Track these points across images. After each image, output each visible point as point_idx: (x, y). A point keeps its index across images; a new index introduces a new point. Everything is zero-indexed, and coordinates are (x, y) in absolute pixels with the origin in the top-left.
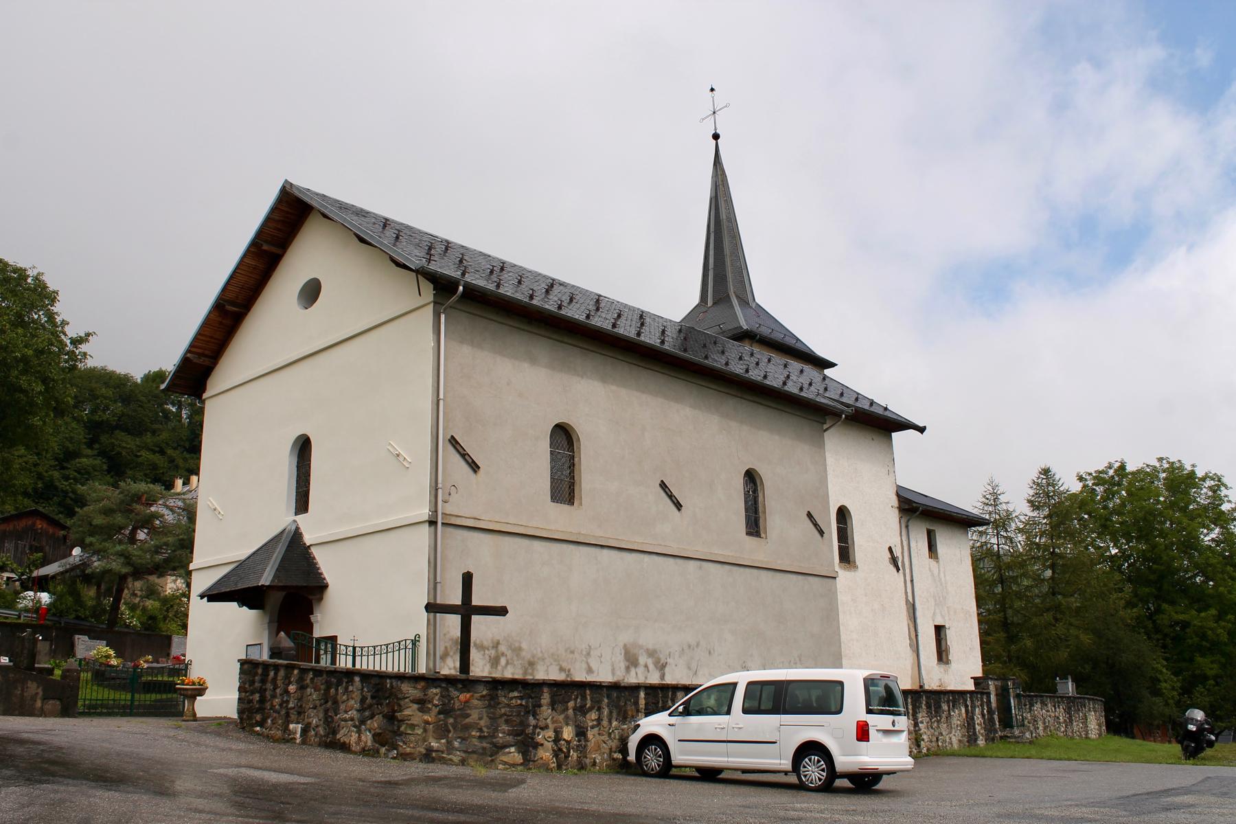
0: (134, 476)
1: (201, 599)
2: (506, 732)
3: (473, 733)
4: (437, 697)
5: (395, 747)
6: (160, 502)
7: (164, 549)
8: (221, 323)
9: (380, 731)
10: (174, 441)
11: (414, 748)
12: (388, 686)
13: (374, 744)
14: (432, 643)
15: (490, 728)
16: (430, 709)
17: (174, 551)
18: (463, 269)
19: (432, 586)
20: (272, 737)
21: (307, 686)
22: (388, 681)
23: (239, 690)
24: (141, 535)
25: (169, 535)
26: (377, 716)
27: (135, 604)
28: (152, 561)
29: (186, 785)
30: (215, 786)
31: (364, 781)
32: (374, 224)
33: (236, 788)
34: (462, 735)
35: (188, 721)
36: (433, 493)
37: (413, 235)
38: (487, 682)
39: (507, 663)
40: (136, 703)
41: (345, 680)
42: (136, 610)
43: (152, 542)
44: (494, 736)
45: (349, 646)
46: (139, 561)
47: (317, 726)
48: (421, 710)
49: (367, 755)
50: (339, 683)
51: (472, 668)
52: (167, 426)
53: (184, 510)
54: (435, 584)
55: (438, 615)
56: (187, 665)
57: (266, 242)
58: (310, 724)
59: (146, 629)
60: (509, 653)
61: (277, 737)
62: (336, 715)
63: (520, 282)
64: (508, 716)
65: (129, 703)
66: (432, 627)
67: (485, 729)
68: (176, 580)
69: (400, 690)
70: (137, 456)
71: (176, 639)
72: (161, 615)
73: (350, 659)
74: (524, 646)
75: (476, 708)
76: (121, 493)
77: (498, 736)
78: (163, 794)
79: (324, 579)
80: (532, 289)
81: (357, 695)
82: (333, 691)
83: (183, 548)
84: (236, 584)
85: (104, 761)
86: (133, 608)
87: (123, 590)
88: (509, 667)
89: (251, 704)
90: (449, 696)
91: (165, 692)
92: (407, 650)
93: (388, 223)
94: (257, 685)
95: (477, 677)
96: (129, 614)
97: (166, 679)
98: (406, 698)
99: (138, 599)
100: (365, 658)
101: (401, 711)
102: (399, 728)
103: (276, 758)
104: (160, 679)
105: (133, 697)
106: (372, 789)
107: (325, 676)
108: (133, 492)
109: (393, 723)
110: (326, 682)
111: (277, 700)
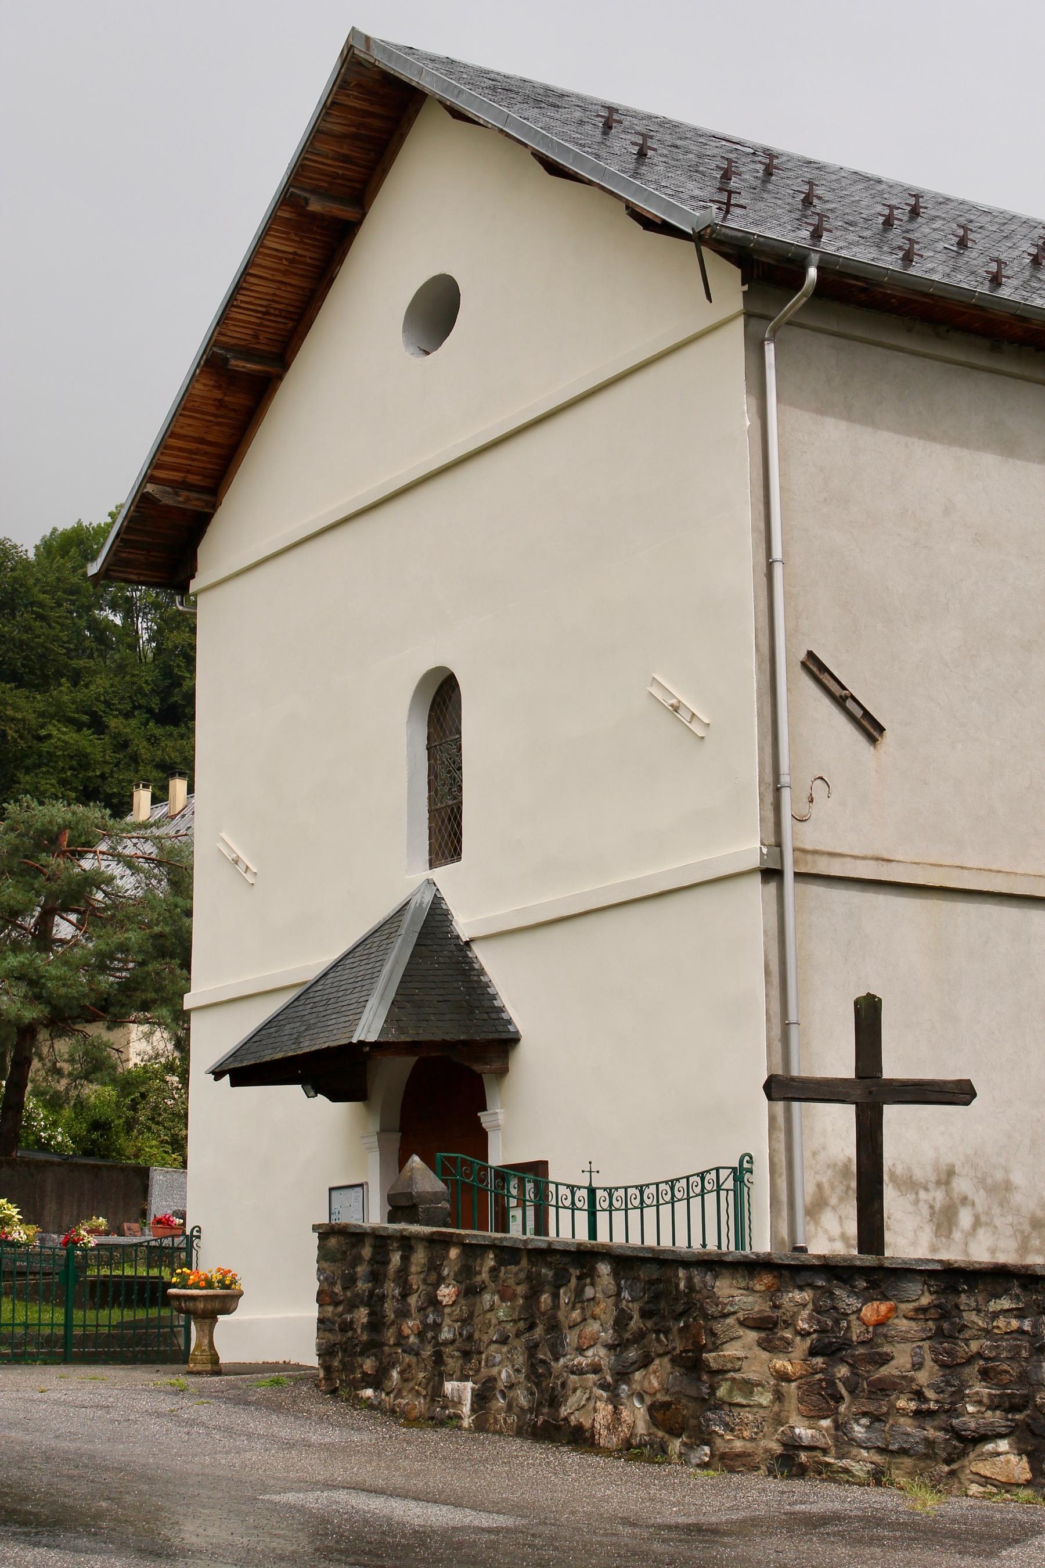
0: (37, 788)
1: (216, 1079)
2: (985, 1400)
3: (901, 1403)
4: (805, 1313)
5: (705, 1438)
6: (103, 847)
7: (119, 960)
8: (220, 404)
9: (667, 1398)
10: (122, 698)
11: (752, 1440)
12: (682, 1285)
13: (654, 1430)
14: (784, 1177)
15: (942, 1392)
16: (788, 1343)
17: (142, 964)
18: (815, 220)
19: (777, 1031)
20: (404, 1414)
21: (483, 1288)
22: (681, 1273)
23: (317, 1301)
24: (64, 929)
25: (128, 925)
26: (657, 1362)
27: (57, 1093)
28: (92, 990)
29: (210, 1532)
30: (278, 1536)
31: (634, 1525)
32: (581, 123)
33: (330, 1542)
34: (871, 1408)
35: (199, 1373)
36: (769, 798)
37: (679, 143)
38: (931, 1273)
39: (977, 1223)
40: (78, 1332)
41: (575, 1272)
42: (61, 1107)
43: (90, 945)
44: (952, 1412)
45: (579, 1188)
46: (63, 991)
47: (511, 1386)
48: (766, 1345)
49: (637, 1458)
50: (560, 1281)
51: (888, 1237)
52: (105, 659)
53: (159, 863)
54: (786, 1026)
55: (796, 1105)
56: (190, 1239)
57: (315, 191)
58: (493, 1379)
59: (87, 1153)
60: (980, 1198)
61: (416, 1413)
62: (557, 1360)
63: (962, 243)
64: (987, 1359)
65: (60, 1331)
66: (782, 1136)
67: (930, 1394)
68: (152, 1033)
69: (712, 1296)
70: (40, 739)
71: (159, 1177)
72: (120, 1117)
73: (582, 1218)
74: (1018, 1178)
75: (905, 1340)
76: (13, 829)
77: (964, 1413)
78: (159, 1555)
79: (510, 1022)
80: (999, 262)
81: (605, 1310)
82: (545, 1298)
83: (164, 957)
84: (297, 1042)
85: (15, 1472)
86: (54, 1102)
87: (29, 1062)
88: (981, 1232)
89: (350, 1334)
90: (835, 1308)
91: (142, 1303)
92: (723, 1194)
93: (615, 117)
94: (362, 1286)
95: (904, 1262)
96: (45, 1118)
97: (142, 1272)
98: (725, 1316)
99: (64, 1082)
100: (618, 1217)
101: (716, 1348)
102: (713, 1389)
103: (417, 1466)
104: (129, 1272)
105: (68, 1316)
106: (657, 1546)
107: (524, 1262)
108: (38, 825)
109: (699, 1379)
110: (529, 1278)
111: (410, 1323)
